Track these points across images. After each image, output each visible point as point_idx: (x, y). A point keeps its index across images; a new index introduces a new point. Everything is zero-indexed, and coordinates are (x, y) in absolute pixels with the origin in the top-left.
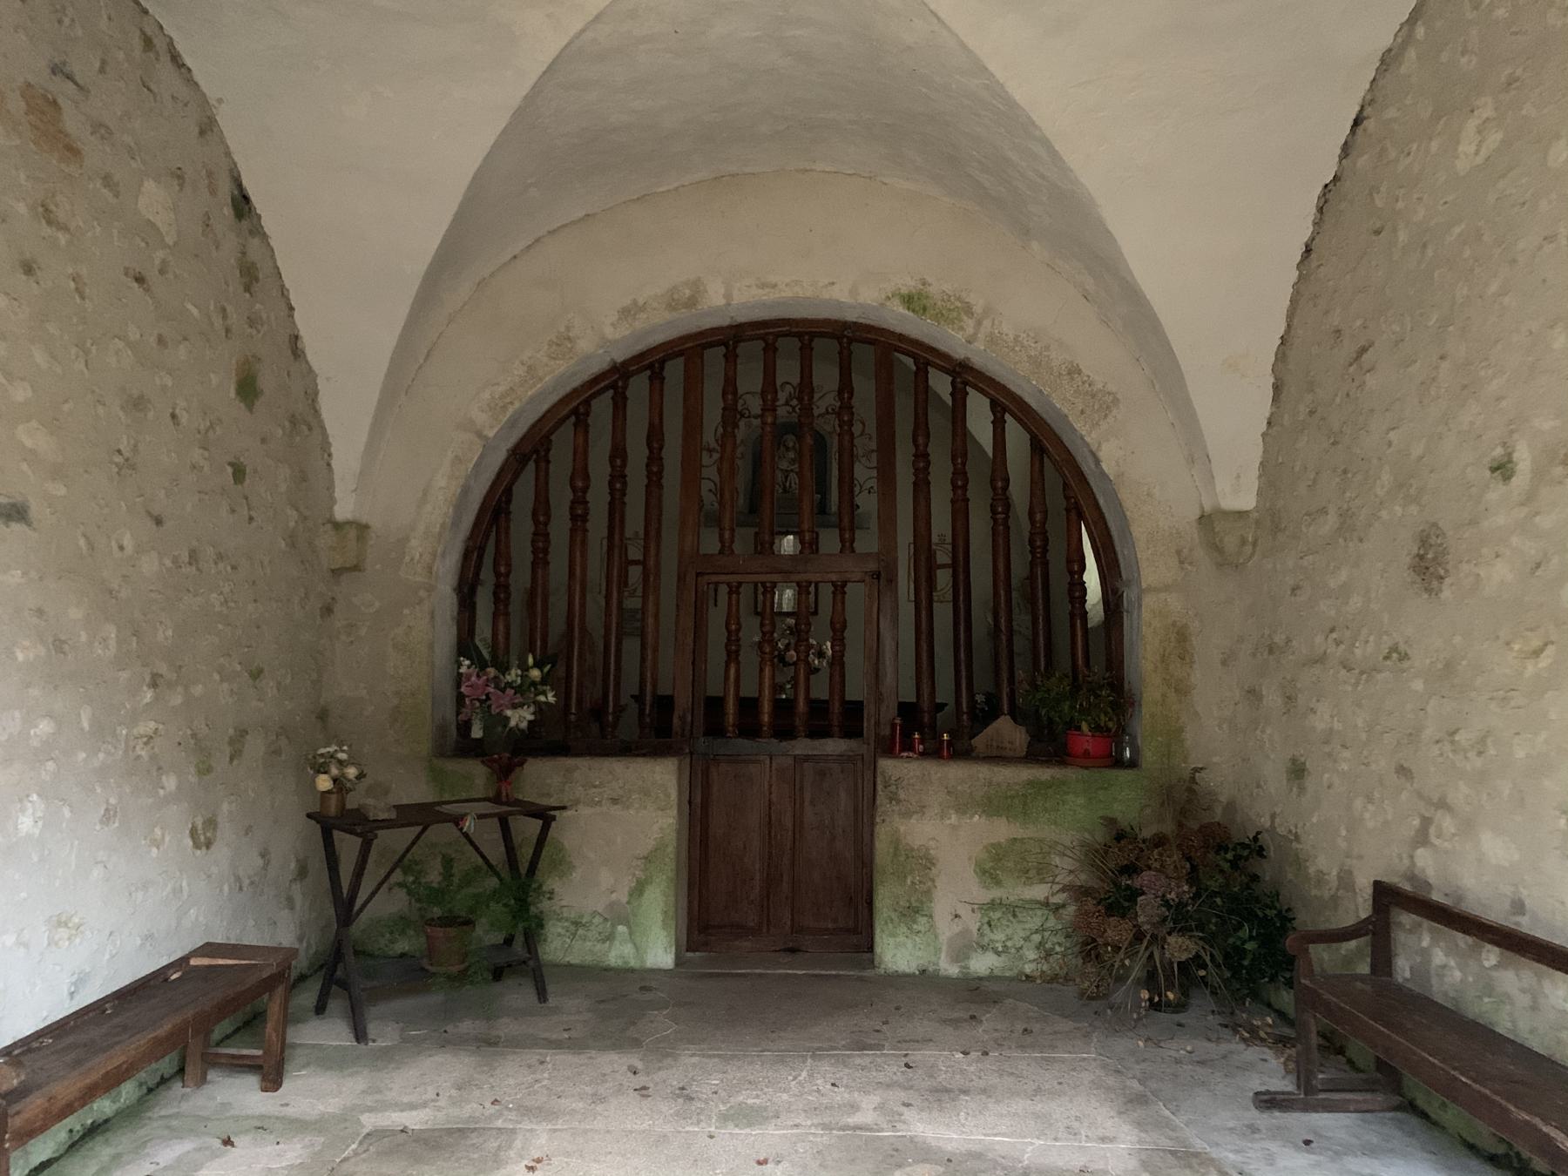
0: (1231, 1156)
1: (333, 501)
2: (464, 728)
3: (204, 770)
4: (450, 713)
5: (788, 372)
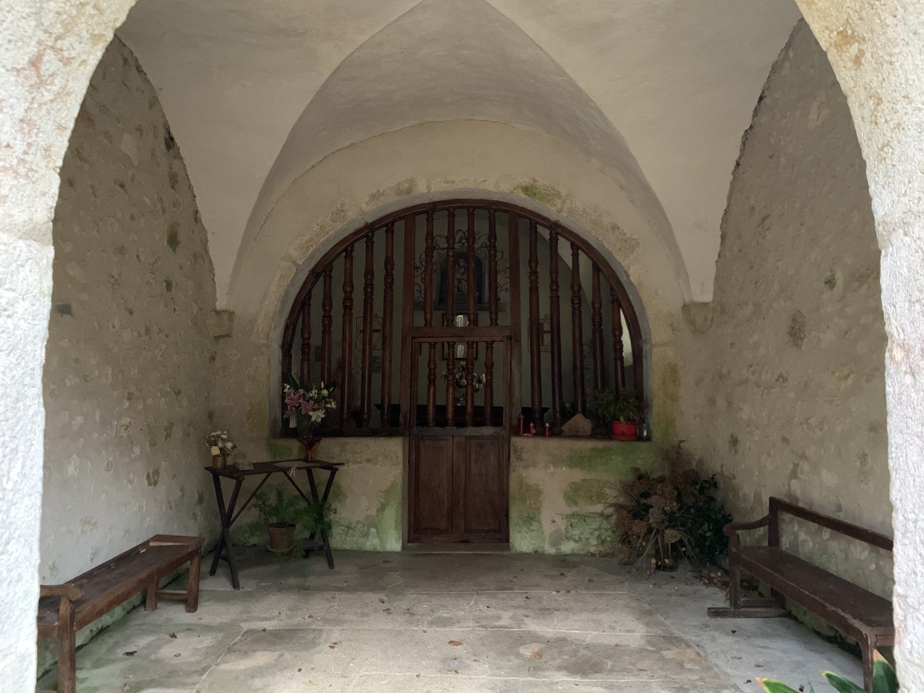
0: (694, 638)
1: (216, 300)
2: (286, 422)
3: (153, 444)
4: (279, 415)
5: (461, 223)
